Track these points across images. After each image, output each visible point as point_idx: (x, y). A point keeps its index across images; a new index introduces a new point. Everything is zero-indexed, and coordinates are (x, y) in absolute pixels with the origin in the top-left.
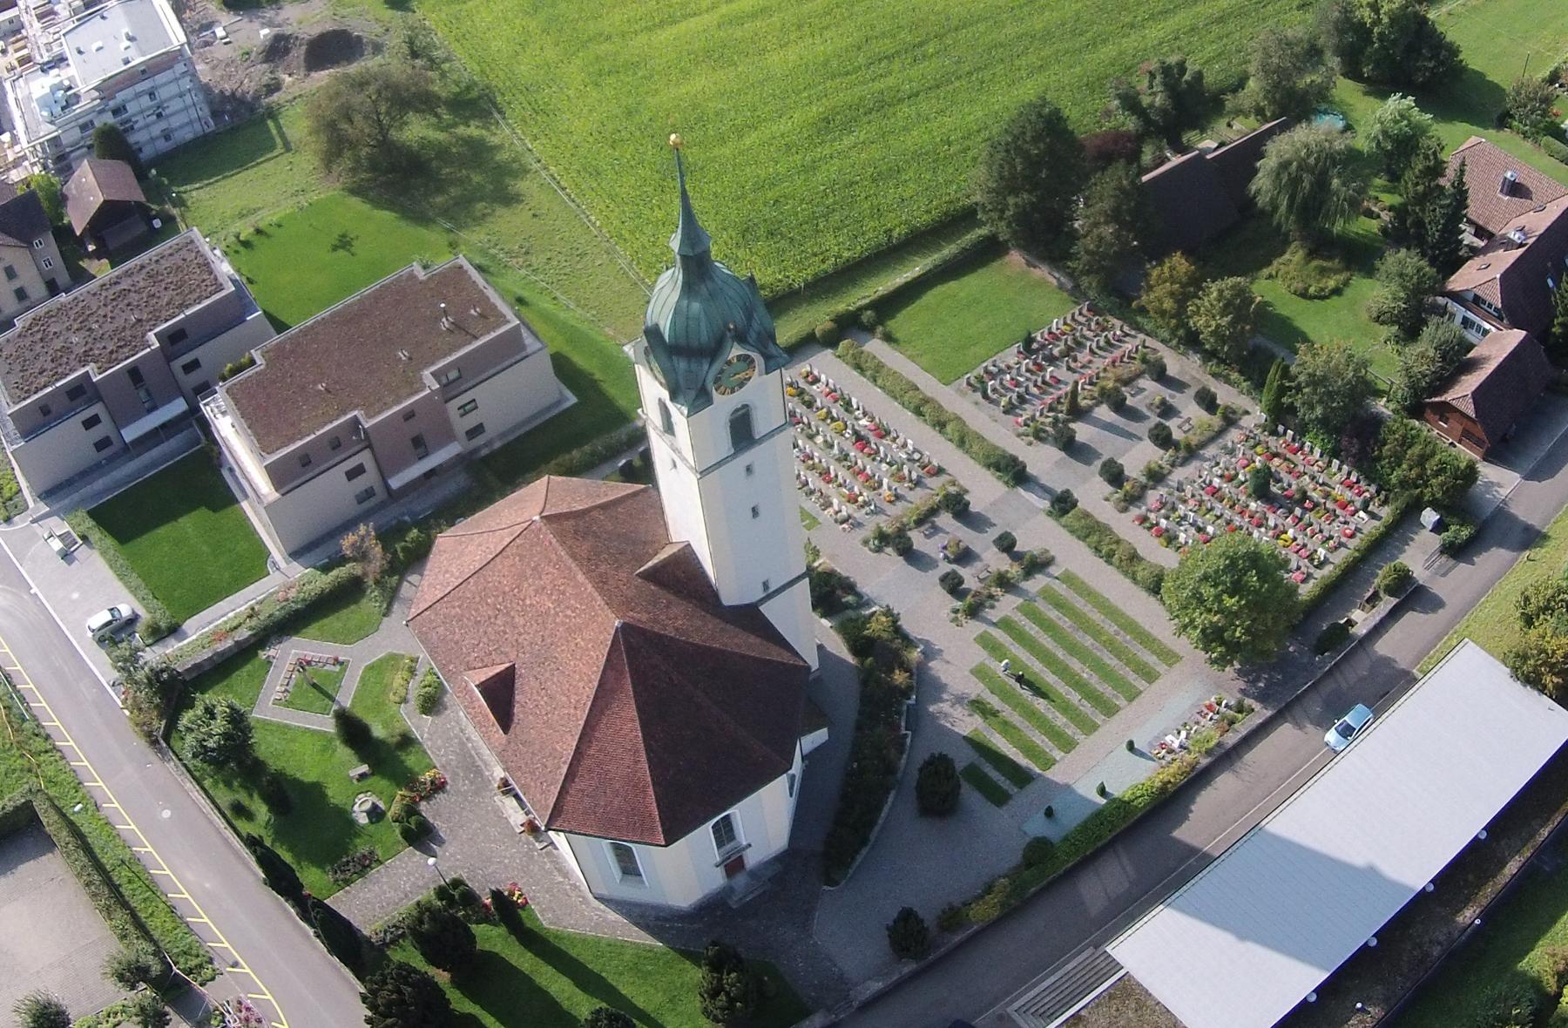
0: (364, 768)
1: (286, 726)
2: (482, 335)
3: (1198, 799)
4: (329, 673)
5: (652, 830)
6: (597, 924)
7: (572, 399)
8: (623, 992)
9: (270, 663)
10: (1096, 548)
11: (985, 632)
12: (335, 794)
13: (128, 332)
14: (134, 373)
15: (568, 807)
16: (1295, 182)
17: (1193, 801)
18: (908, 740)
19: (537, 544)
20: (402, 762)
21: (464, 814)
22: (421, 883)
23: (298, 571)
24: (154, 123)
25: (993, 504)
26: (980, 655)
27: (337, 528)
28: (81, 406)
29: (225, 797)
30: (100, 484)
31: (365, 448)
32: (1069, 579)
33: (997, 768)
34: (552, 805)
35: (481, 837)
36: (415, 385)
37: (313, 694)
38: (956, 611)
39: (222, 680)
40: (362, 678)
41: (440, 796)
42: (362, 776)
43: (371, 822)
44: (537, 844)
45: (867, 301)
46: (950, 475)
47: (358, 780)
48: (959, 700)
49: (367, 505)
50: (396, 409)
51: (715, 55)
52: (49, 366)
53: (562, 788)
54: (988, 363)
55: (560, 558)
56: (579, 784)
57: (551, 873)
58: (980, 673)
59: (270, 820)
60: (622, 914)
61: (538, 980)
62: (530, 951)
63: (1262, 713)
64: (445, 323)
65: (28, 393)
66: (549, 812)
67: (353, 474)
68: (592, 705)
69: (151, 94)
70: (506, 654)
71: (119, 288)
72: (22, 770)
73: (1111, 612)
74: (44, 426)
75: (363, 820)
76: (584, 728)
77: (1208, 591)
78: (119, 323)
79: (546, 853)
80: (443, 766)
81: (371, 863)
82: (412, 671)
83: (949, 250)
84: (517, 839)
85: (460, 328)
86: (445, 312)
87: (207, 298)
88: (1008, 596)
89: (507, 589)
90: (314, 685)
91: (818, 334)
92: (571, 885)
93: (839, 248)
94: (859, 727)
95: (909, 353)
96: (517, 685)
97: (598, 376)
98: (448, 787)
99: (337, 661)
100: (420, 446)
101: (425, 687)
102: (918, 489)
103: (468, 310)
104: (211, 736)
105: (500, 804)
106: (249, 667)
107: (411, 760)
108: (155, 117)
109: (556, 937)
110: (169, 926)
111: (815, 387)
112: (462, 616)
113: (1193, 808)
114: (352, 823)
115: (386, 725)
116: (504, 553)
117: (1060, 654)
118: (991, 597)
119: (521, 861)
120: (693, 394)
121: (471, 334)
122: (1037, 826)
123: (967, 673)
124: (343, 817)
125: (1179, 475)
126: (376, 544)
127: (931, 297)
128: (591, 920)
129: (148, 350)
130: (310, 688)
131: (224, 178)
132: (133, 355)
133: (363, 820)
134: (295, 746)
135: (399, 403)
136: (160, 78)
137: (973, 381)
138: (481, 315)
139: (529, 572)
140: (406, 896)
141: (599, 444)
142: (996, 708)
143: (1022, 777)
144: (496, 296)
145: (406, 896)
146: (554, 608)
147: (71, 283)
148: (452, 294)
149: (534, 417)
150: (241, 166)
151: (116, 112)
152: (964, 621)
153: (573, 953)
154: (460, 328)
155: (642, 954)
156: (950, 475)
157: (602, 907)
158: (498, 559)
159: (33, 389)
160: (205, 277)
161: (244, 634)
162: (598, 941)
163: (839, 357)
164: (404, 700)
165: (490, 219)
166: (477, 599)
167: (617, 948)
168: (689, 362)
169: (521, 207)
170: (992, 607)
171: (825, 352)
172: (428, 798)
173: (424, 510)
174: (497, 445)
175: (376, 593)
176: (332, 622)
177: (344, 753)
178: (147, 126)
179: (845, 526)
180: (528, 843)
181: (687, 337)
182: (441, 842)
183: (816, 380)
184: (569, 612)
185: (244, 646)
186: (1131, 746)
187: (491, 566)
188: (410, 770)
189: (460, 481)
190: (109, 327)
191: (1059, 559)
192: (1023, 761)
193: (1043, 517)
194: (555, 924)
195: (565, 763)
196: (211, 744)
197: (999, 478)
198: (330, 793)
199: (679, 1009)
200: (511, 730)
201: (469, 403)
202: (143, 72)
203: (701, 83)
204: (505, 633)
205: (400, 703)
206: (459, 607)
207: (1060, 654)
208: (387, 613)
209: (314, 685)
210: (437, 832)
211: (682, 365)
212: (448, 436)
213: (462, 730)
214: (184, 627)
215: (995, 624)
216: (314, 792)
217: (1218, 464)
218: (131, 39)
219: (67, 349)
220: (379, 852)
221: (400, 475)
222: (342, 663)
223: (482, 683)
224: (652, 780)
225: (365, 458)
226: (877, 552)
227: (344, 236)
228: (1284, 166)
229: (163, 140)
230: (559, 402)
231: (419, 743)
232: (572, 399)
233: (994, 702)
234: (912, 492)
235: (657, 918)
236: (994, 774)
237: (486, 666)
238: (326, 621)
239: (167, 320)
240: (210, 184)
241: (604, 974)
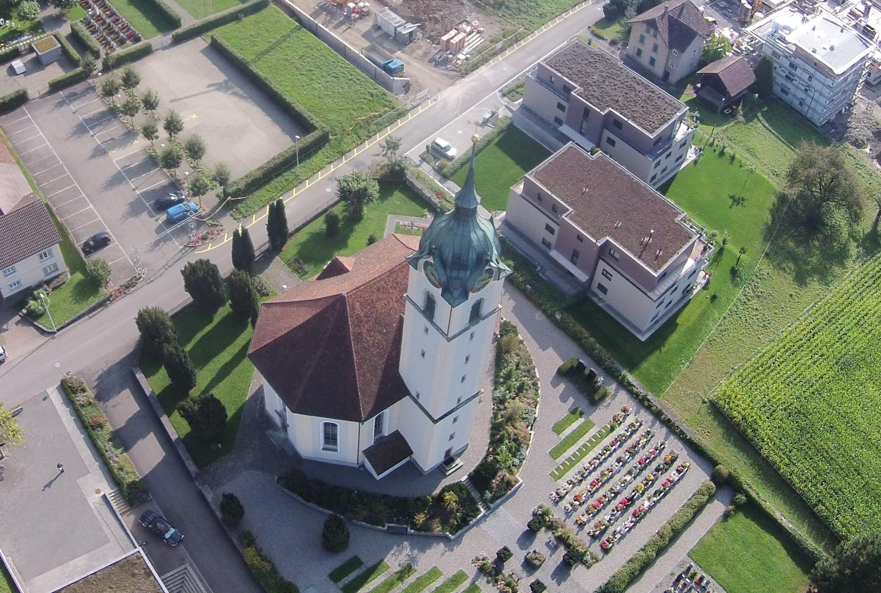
2: (643, 260)
11: (468, 577)
13: (608, 99)
14: (587, 111)
18: (380, 527)
24: (801, 90)
25: (578, 584)
26: (448, 573)
28: (564, 96)
30: (538, 129)
33: (358, 577)
39: (408, 197)
45: (754, 495)
46: (603, 557)
48: (413, 559)
52: (575, 71)
54: (707, 578)
58: (434, 573)
65: (554, 67)
69: (810, 78)
71: (636, 86)
72: (342, 127)
74: (546, 84)
78: (613, 93)
83: (810, 543)
86: (651, 235)
87: (643, 127)
94: (385, 496)
95: (715, 529)
97: (664, 349)
102: (589, 538)
108: (803, 88)
110: (263, 199)
111: (675, 472)
121: (642, 254)
123: (434, 565)
127: (768, 538)
129: (599, 111)
131: (777, 137)
132: (593, 105)
136: (818, 75)
137: (692, 571)
141: (605, 354)
142: (405, 581)
144: (671, 262)
147: (674, 84)
148: (669, 238)
149: (618, 314)
150: (789, 142)
151: (792, 65)
152: (476, 564)
156: (603, 557)
159: (556, 68)
160: (656, 122)
165: (781, 273)
169: (797, 287)
170: (488, 582)
171: (706, 475)
178: (797, 87)
179: (554, 494)
190: (609, 89)
202: (816, 64)
214: (449, 181)
215: (473, 583)
218: (832, 49)
219: (588, 75)
221: (559, 255)
226: (533, 514)
227: (743, 199)
229: (799, 102)
230: (639, 331)
233: (411, 579)
234: (586, 534)
236: (352, 576)
239: (621, 114)
240: (771, 131)
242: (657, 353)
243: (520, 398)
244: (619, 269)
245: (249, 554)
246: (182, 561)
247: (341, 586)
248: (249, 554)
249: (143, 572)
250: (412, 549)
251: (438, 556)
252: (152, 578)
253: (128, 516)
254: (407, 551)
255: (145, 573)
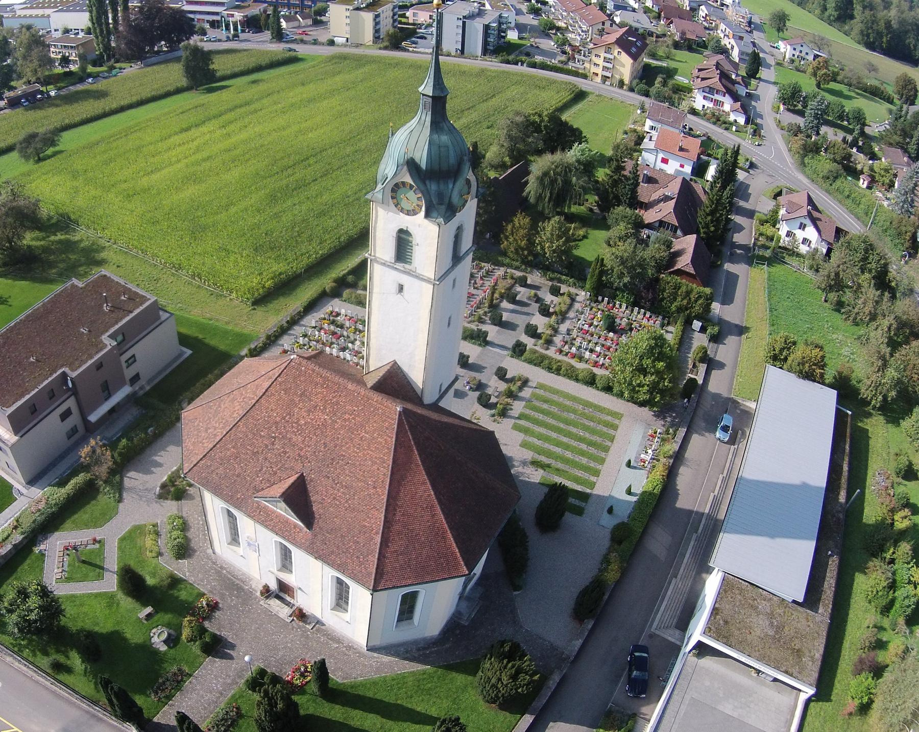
0: (149, 610)
1: (73, 596)
2: (134, 309)
3: (678, 483)
4: (92, 552)
5: (456, 566)
6: (377, 668)
7: (189, 352)
8: (419, 709)
9: (44, 555)
10: (548, 368)
12: (133, 635)
15: (388, 568)
16: (553, 182)
17: (676, 485)
19: (299, 376)
20: (177, 597)
21: (242, 621)
22: (229, 681)
23: (36, 493)
26: (520, 437)
27: (56, 459)
29: (45, 662)
31: (71, 396)
32: (540, 386)
34: (374, 571)
35: (262, 634)
36: (100, 346)
37: (84, 568)
38: (493, 416)
40: (120, 548)
41: (217, 614)
42: (149, 616)
43: (169, 647)
44: (307, 626)
47: (146, 620)
48: (524, 463)
49: (73, 439)
50: (90, 362)
51: (192, 178)
53: (380, 553)
55: (326, 379)
56: (393, 547)
57: (327, 643)
58: (524, 445)
59: (86, 668)
60: (392, 655)
61: (352, 723)
62: (337, 704)
63: (682, 432)
64: (106, 308)
66: (373, 577)
67: (65, 416)
68: (390, 481)
70: (292, 468)
73: (574, 399)
75: (163, 648)
76: (388, 501)
77: (647, 362)
79: (316, 630)
80: (211, 592)
81: (182, 678)
82: (157, 534)
84: (290, 627)
85: (118, 308)
88: (515, 402)
89: (278, 419)
90: (84, 562)
91: (328, 290)
92: (345, 647)
93: (316, 251)
96: (310, 488)
97: (201, 336)
98: (220, 606)
99: (95, 541)
100: (107, 391)
101: (175, 539)
103: (120, 296)
104: (32, 611)
105: (266, 606)
106: (28, 561)
107: (183, 595)
109: (352, 687)
111: (339, 318)
112: (238, 453)
113: (678, 488)
114: (156, 652)
115: (154, 575)
116: (267, 394)
117: (562, 425)
118: (508, 404)
119: (300, 641)
120: (443, 207)
122: (609, 522)
123: (519, 447)
124: (146, 648)
125: (563, 328)
126: (106, 449)
128: (371, 666)
130: (81, 564)
133: (163, 648)
134: (85, 609)
135: (92, 358)
138: (129, 299)
139: (297, 400)
140: (221, 694)
143: (584, 497)
145: (221, 694)
146: (331, 418)
149: (159, 373)
153: (370, 694)
154: (118, 308)
155: (419, 679)
157: (376, 655)
158: (262, 400)
161: (17, 538)
162: (385, 680)
163: (345, 301)
164: (160, 554)
166: (250, 436)
167: (400, 681)
168: (438, 183)
172: (208, 618)
173: (115, 435)
174: (148, 388)
175: (108, 489)
176: (83, 515)
177: (127, 602)
180: (299, 627)
181: (440, 164)
182: (233, 647)
183: (338, 314)
184: (347, 416)
185: (20, 547)
186: (629, 464)
187: (257, 406)
188: (186, 602)
189: (133, 413)
191: (530, 378)
192: (579, 488)
193: (509, 358)
194: (346, 678)
195: (377, 533)
196: (33, 617)
197: (474, 343)
198: (128, 636)
199: (462, 707)
200: (315, 526)
201: (130, 358)
203: (191, 191)
204: (285, 453)
205: (158, 557)
206: (234, 447)
207: (562, 425)
208: (120, 500)
209: (84, 562)
210: (226, 639)
211: (433, 187)
212: (122, 384)
213: (214, 563)
215: (518, 418)
216: (115, 639)
217: (579, 320)
220: (186, 669)
222: (100, 542)
223: (284, 493)
224: (449, 526)
225: (71, 403)
228: (546, 174)
231: (185, 580)
232: (189, 352)
235: (418, 650)
237: (274, 484)
238: (76, 516)
241: (399, 702)
242: (207, 341)
243: (667, 47)
244: (132, 343)
245: (612, 576)
246: (652, 636)
247: (584, 504)
248: (612, 576)
249: (718, 617)
250: (514, 466)
251: (509, 447)
252: (717, 606)
253: (646, 715)
254: (520, 469)
255: (717, 614)
